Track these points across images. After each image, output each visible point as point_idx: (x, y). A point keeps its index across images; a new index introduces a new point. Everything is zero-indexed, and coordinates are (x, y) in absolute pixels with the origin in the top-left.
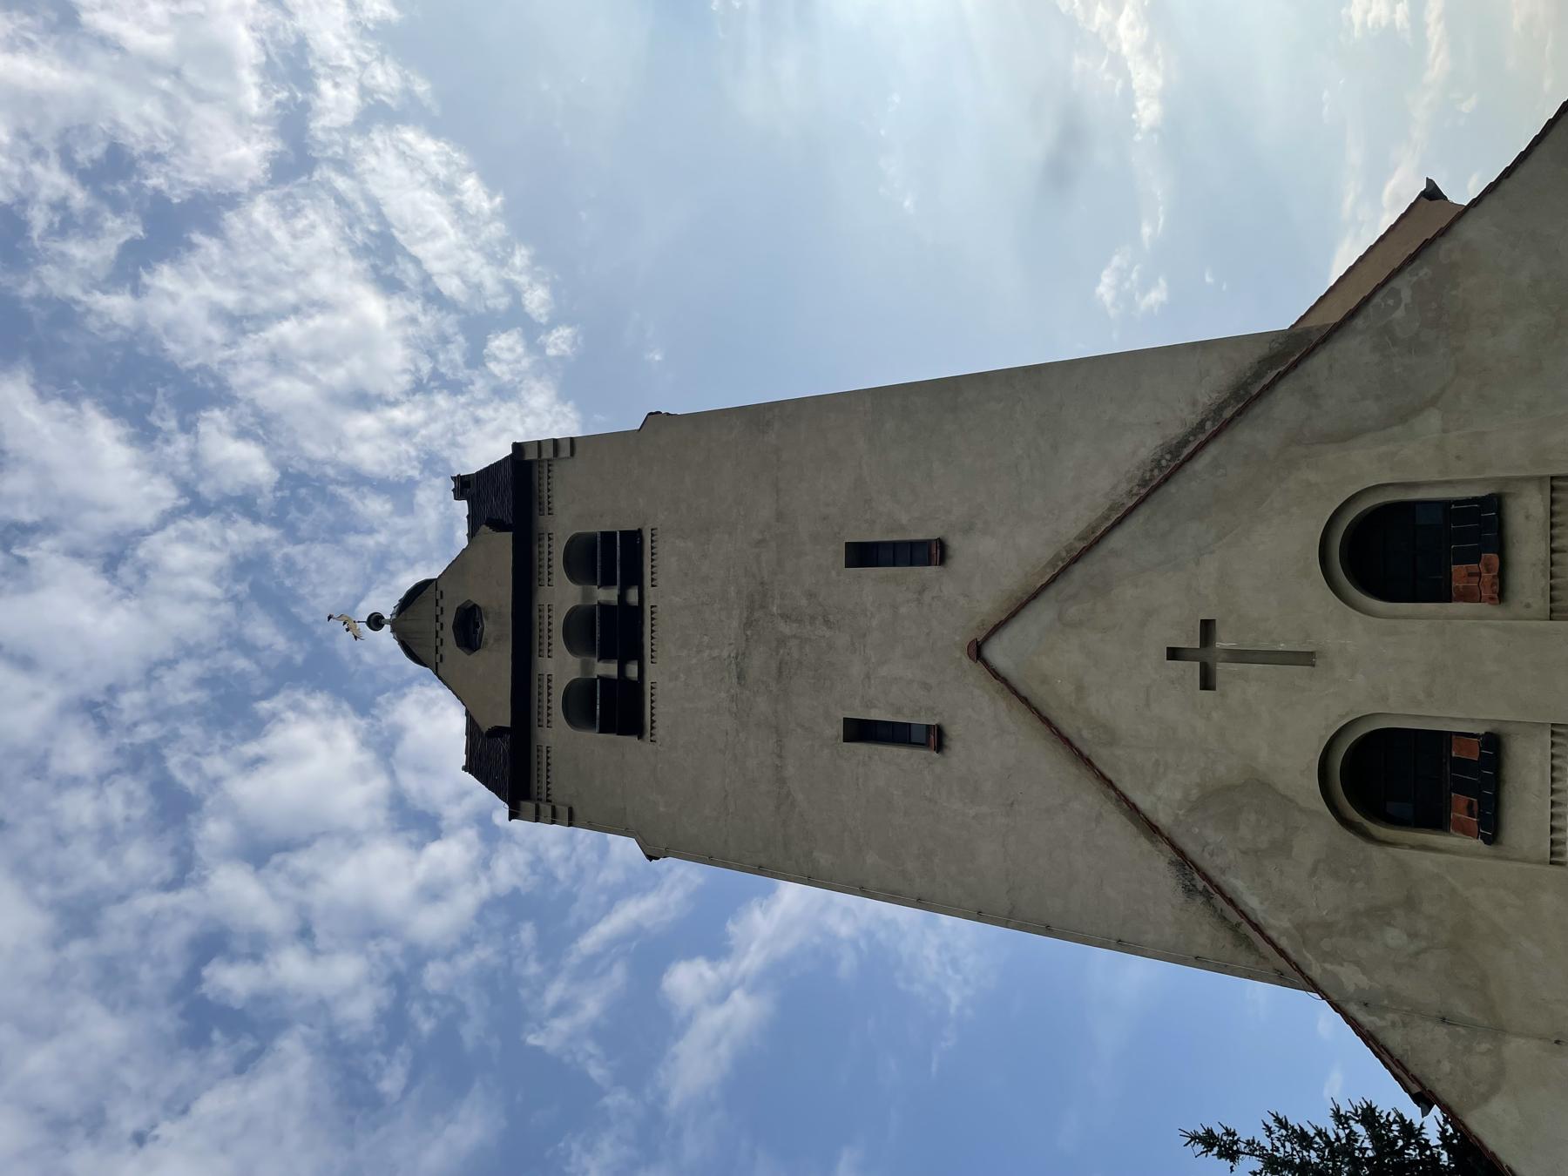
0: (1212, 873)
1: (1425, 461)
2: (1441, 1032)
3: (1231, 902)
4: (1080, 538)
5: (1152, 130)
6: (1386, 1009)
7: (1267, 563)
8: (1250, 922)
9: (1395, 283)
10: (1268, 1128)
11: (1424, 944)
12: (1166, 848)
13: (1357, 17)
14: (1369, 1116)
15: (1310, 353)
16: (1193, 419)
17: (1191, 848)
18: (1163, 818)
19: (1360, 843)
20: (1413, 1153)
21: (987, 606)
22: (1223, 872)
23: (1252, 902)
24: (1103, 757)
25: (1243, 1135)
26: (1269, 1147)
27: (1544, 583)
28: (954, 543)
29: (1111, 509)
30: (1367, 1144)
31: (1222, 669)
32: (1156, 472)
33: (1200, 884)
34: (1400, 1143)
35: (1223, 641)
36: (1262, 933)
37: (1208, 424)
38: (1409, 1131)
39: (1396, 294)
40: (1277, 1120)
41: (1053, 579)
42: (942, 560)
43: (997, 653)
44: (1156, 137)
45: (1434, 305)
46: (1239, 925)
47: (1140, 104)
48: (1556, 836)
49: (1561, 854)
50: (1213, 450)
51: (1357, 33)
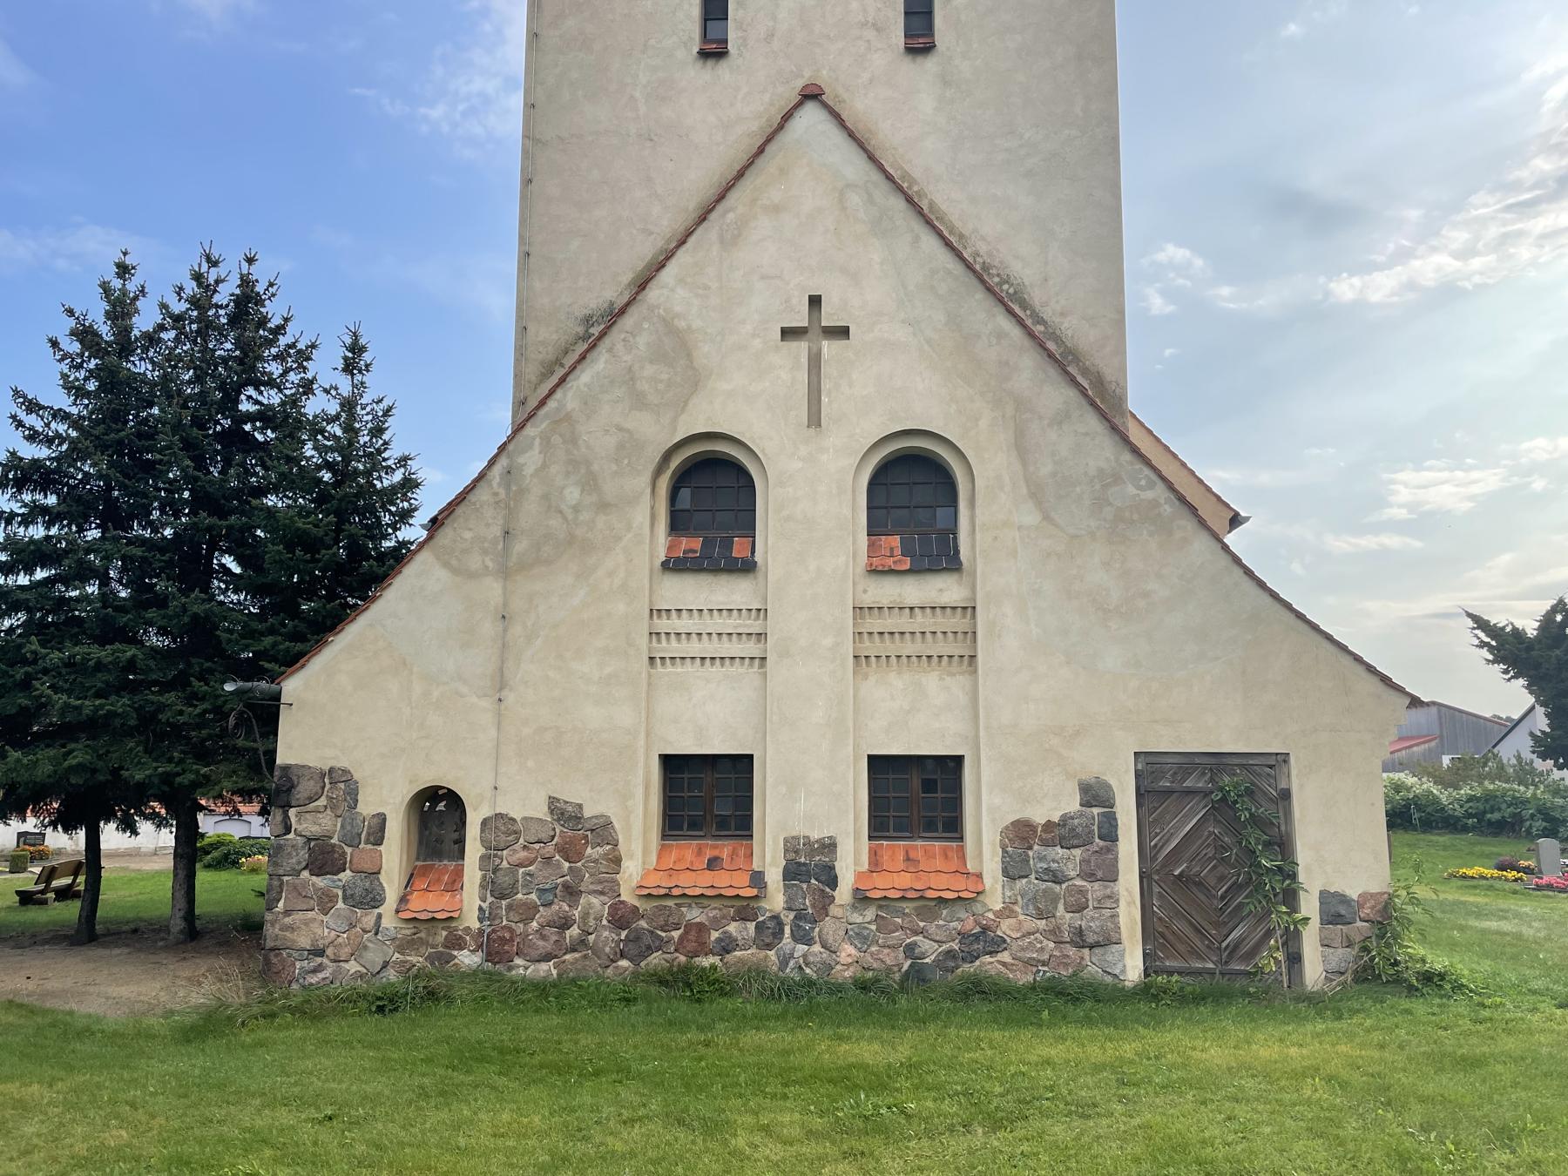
0: (607, 341)
1: (990, 515)
2: (497, 531)
3: (583, 357)
4: (932, 204)
5: (1327, 294)
6: (508, 488)
7: (899, 384)
8: (567, 374)
9: (1160, 485)
10: (380, 401)
11: (570, 517)
12: (626, 298)
13: (1401, 476)
14: (410, 484)
15: (1103, 416)
16: (1047, 314)
17: (628, 321)
18: (653, 294)
19: (651, 467)
20: (387, 519)
21: (862, 106)
22: (610, 350)
23: (584, 378)
24: (708, 234)
25: (368, 378)
26: (363, 401)
27: (885, 603)
28: (930, 64)
29: (961, 236)
30: (386, 483)
31: (801, 348)
32: (997, 280)
33: (595, 331)
34: (393, 509)
35: (828, 347)
36: (558, 385)
37: (1041, 328)
38: (405, 516)
39: (1151, 486)
40: (390, 409)
41: (889, 177)
42: (911, 51)
43: (811, 115)
44: (1320, 297)
45: (1135, 517)
46: (562, 365)
47: (1356, 281)
48: (674, 613)
49: (659, 617)
50: (1015, 332)
51: (1385, 476)
